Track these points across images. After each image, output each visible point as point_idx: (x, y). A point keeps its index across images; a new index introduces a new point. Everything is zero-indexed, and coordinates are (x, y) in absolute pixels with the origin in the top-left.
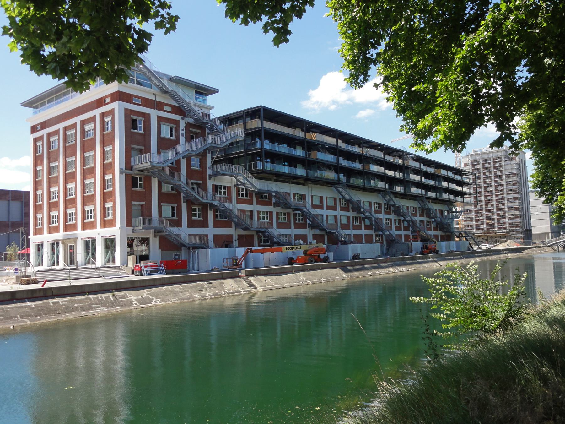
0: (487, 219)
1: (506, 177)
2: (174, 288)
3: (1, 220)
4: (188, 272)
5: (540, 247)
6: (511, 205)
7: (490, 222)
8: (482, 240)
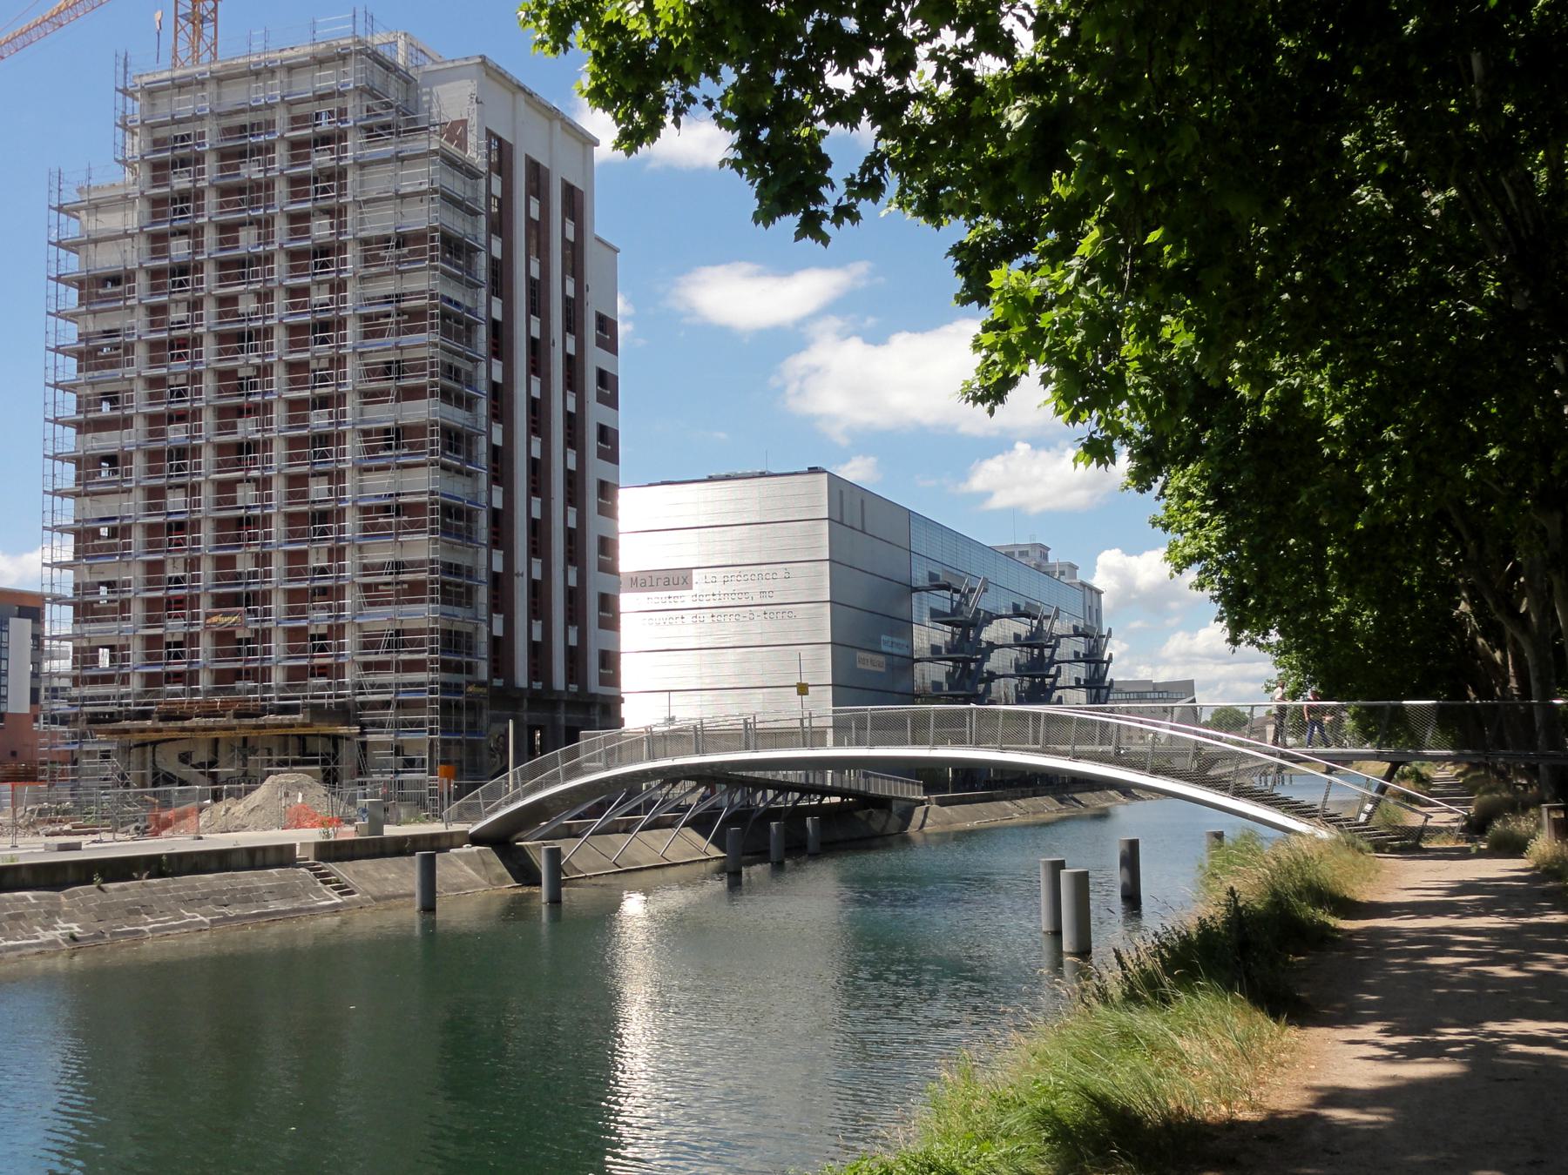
0: (220, 601)
1: (368, 260)
2: (220, 878)
3: (9, 583)
4: (936, 726)
5: (282, 856)
6: (380, 485)
7: (241, 622)
8: (185, 771)
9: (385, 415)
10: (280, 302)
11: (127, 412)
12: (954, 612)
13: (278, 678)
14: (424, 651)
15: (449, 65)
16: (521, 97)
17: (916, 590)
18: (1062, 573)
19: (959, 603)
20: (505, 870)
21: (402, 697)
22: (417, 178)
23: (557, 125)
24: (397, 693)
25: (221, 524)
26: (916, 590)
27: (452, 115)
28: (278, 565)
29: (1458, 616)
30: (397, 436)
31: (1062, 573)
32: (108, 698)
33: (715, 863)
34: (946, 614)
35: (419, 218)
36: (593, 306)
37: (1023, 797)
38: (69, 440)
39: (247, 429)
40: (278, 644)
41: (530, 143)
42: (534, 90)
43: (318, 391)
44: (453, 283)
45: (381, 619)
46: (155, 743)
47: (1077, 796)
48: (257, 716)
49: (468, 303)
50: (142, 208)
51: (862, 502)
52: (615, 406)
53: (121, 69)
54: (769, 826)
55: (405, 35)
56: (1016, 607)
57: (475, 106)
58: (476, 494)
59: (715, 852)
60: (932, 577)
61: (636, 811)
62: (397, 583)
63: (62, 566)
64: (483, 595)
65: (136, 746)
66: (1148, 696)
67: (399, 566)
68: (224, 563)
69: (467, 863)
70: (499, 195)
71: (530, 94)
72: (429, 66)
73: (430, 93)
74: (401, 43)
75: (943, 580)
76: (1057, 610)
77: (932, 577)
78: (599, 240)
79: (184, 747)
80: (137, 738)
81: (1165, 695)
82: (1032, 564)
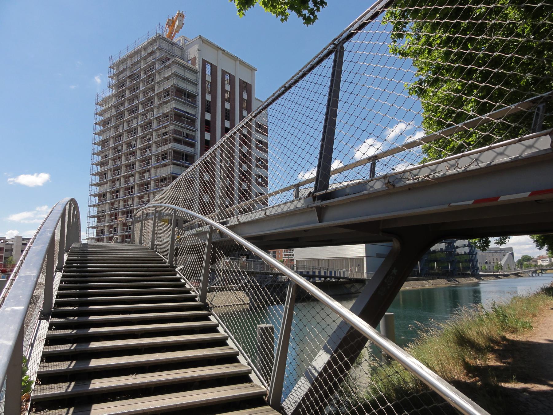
15: (192, 41)
23: (238, 62)
27: (191, 56)
35: (167, 85)
37: (433, 279)
38: (98, 169)
41: (224, 65)
42: (225, 49)
47: (457, 279)
49: (193, 113)
55: (183, 36)
57: (198, 51)
61: (225, 266)
66: (499, 251)
70: (246, 99)
71: (223, 51)
78: (256, 99)
81: (504, 251)
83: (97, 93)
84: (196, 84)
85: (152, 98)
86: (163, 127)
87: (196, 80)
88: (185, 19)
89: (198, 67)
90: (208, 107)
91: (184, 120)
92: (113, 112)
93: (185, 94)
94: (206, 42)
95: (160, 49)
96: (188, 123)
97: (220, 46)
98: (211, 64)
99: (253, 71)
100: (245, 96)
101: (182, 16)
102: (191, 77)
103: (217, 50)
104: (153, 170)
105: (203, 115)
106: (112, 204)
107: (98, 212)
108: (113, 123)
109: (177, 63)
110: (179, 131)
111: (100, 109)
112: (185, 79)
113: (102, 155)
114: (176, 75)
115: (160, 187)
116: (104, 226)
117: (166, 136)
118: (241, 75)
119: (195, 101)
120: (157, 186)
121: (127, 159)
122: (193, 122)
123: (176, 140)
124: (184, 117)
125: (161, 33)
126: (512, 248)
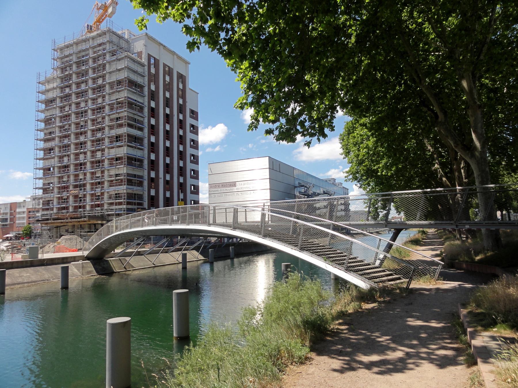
9: (114, 132)
10: (90, 102)
11: (103, 147)
12: (305, 192)
13: (88, 208)
14: (122, 199)
16: (162, 47)
17: (296, 187)
18: (339, 185)
19: (306, 190)
20: (93, 269)
21: (117, 212)
22: (121, 65)
23: (175, 57)
24: (116, 211)
25: (76, 165)
26: (296, 187)
28: (88, 176)
29: (435, 170)
30: (118, 138)
31: (339, 185)
32: (47, 214)
33: (202, 261)
34: (303, 193)
35: (122, 75)
36: (189, 106)
38: (42, 145)
39: (82, 139)
40: (88, 198)
41: (165, 59)
42: (166, 45)
43: (97, 126)
44: (135, 95)
45: (113, 190)
46: (60, 227)
48: (80, 218)
50: (59, 80)
51: (279, 165)
52: (197, 134)
53: (53, 44)
54: (209, 251)
56: (324, 192)
58: (144, 155)
59: (201, 257)
60: (299, 183)
62: (116, 180)
63: (40, 179)
64: (146, 183)
65: (55, 227)
67: (117, 175)
68: (77, 176)
69: (76, 267)
71: (165, 46)
72: (133, 37)
73: (133, 45)
74: (126, 33)
75: (303, 184)
76: (335, 192)
77: (299, 183)
78: (190, 89)
79: (67, 228)
80: (55, 225)
82: (331, 183)
83: (38, 72)
84: (144, 76)
85: (71, 75)
86: (116, 113)
87: (144, 72)
88: (117, 6)
89: (144, 60)
90: (153, 96)
91: (136, 108)
92: (57, 93)
93: (136, 85)
94: (151, 39)
95: (110, 42)
96: (139, 111)
97: (162, 42)
98: (154, 58)
99: (187, 64)
100: (181, 86)
101: (115, 3)
102: (140, 70)
103: (159, 46)
104: (106, 150)
105: (149, 103)
106: (60, 178)
107: (44, 184)
108: (58, 102)
109: (128, 57)
110: (132, 118)
111: (43, 88)
112: (135, 72)
113: (46, 131)
114: (128, 68)
115: (116, 166)
116: (53, 197)
117: (120, 122)
118: (178, 68)
119: (143, 90)
120: (111, 164)
121: (77, 138)
122: (141, 109)
123: (130, 126)
124: (136, 105)
125: (111, 27)
126: (354, 191)
